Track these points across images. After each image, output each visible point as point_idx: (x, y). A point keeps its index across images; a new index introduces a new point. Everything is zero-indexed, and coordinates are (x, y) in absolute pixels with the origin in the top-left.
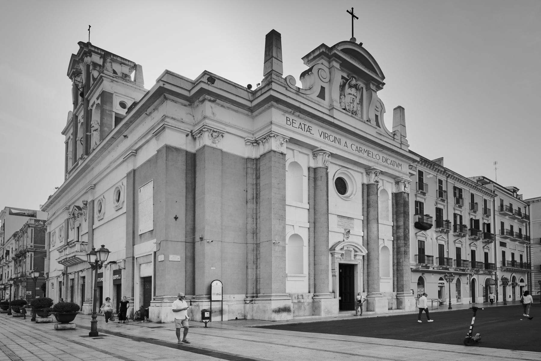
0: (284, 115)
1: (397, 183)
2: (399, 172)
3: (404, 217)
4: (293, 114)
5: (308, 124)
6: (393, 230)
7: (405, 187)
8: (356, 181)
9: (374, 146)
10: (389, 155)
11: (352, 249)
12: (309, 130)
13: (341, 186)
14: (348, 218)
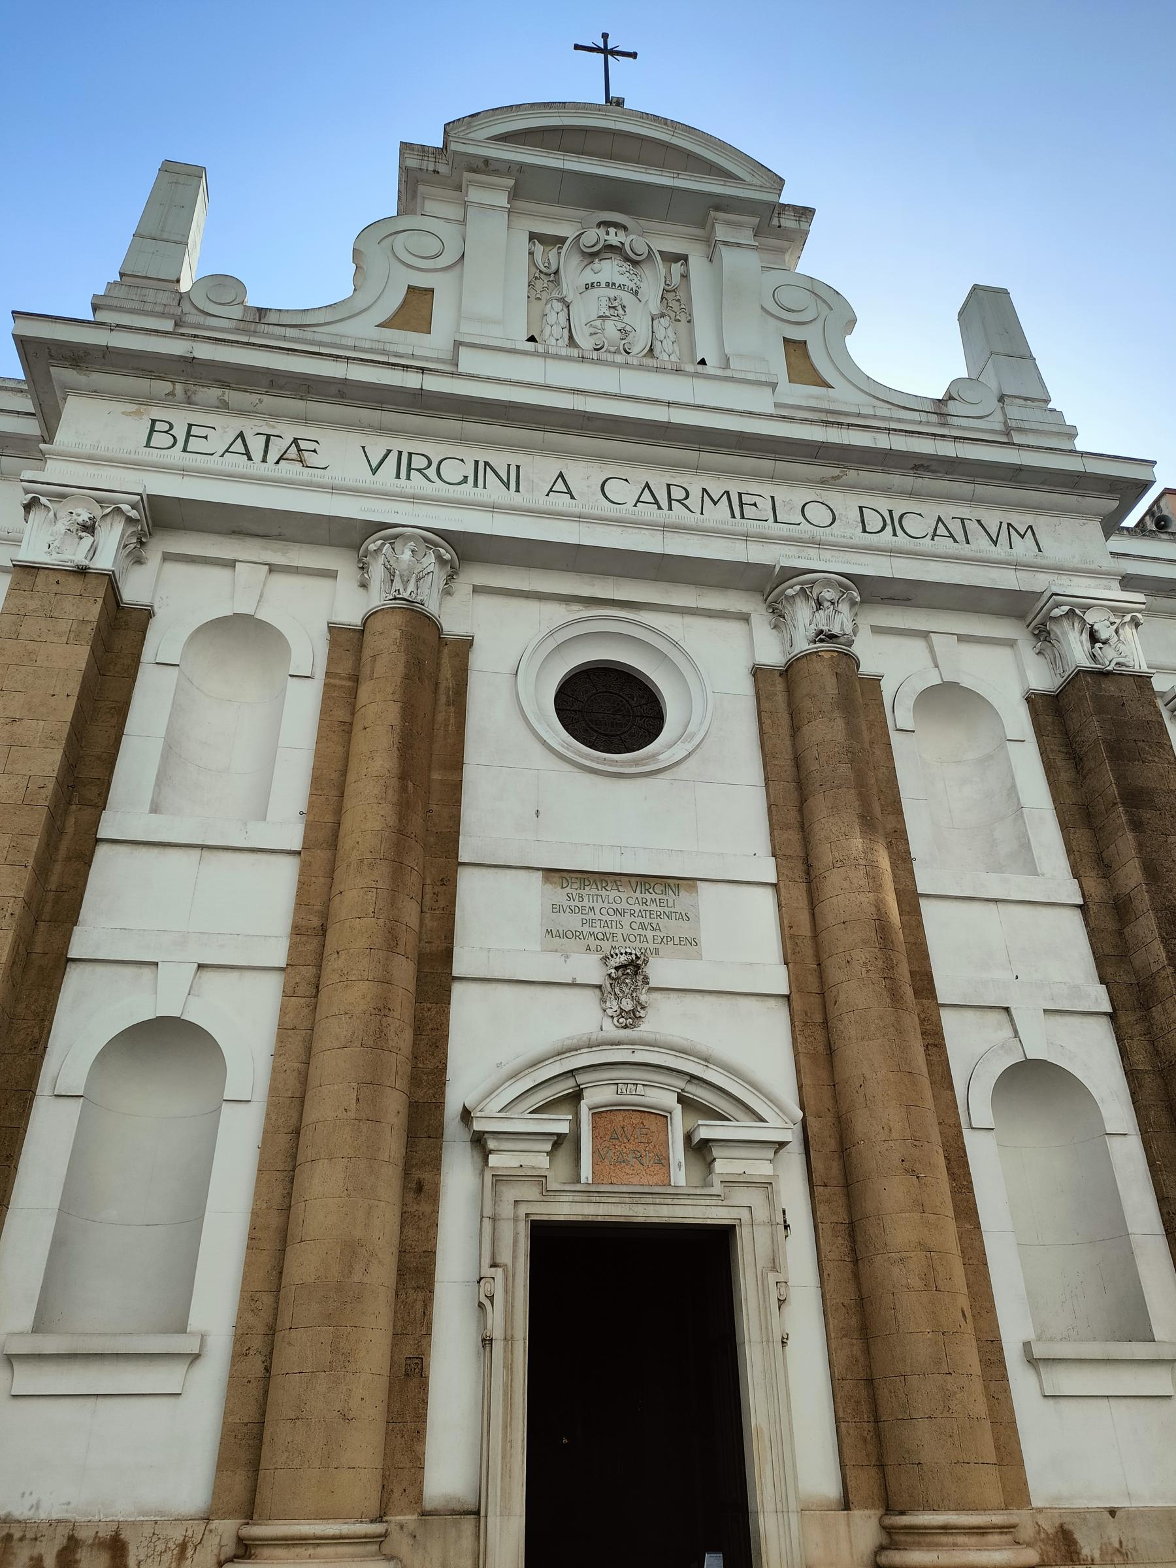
0: (138, 413)
1: (1042, 634)
2: (1017, 565)
3: (1137, 826)
4: (189, 401)
5: (289, 432)
6: (1093, 934)
7: (1094, 638)
8: (710, 669)
9: (767, 465)
10: (912, 494)
11: (668, 1100)
12: (298, 452)
13: (610, 710)
14: (645, 881)
